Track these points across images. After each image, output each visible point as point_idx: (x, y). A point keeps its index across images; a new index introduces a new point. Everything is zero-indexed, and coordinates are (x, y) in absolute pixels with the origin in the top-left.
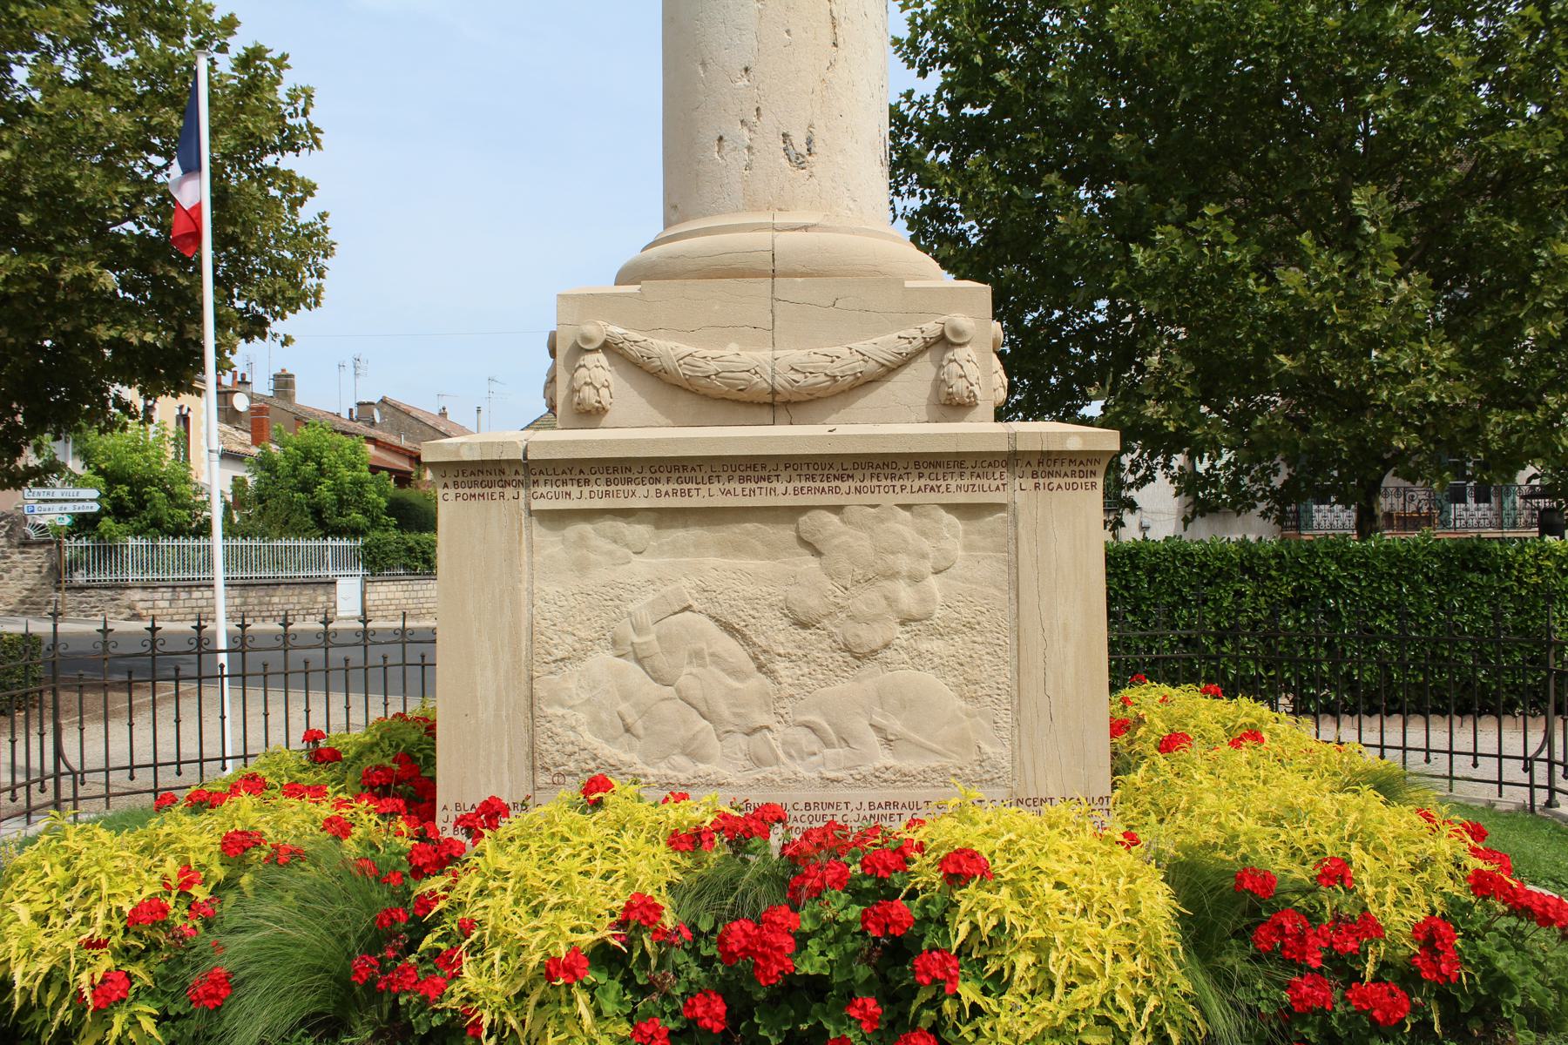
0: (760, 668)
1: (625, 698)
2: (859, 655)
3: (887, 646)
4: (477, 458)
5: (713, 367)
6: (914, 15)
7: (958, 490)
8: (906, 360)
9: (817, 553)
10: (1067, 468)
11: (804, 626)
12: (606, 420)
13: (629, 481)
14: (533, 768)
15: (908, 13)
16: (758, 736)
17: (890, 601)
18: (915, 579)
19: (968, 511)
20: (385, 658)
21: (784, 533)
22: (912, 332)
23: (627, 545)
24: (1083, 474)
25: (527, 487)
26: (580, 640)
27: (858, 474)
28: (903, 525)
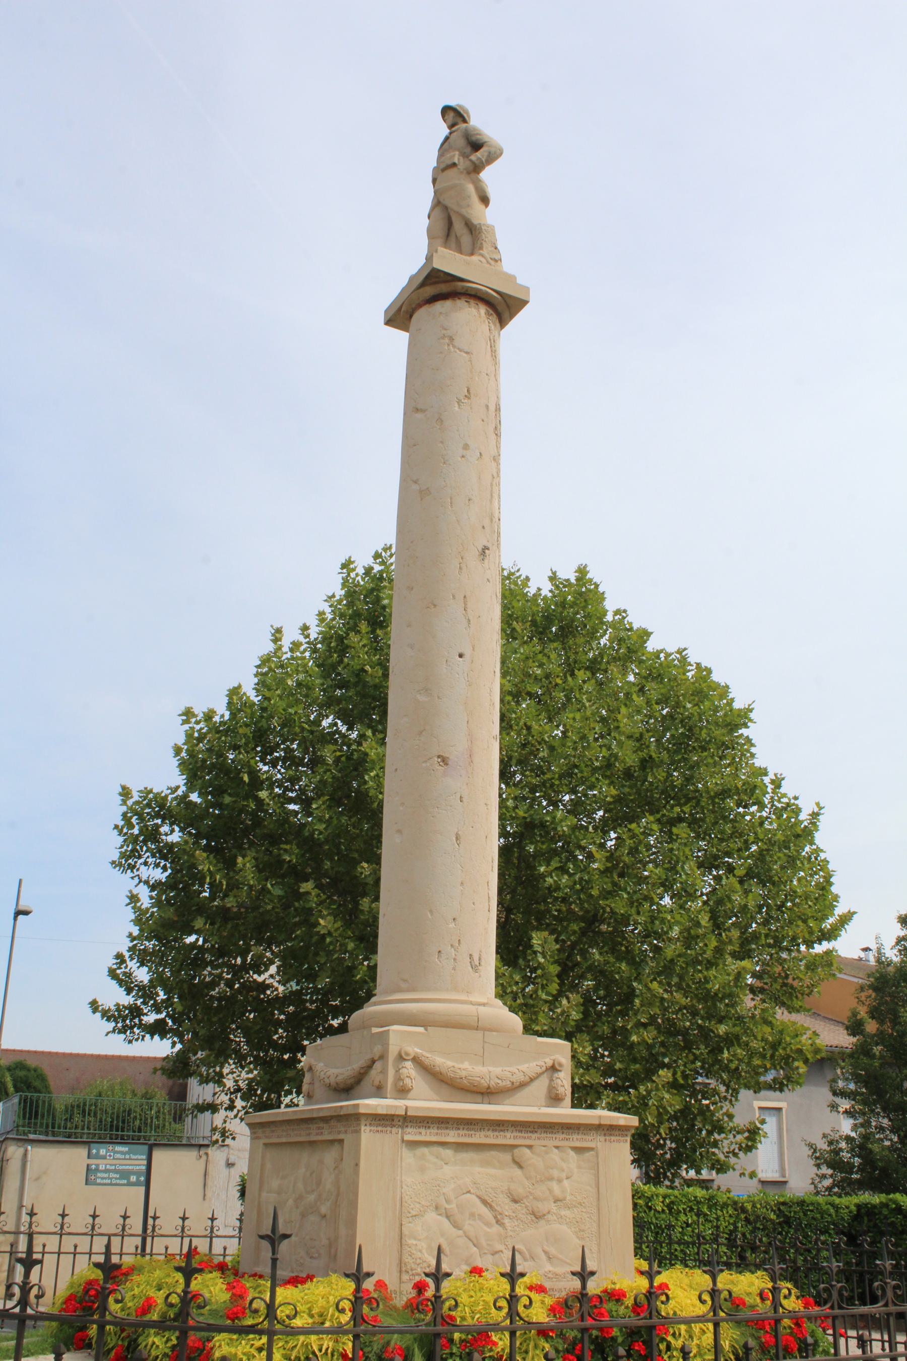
0: (497, 1222)
1: (442, 1235)
2: (537, 1216)
3: (549, 1213)
4: (385, 1112)
5: (463, 1074)
6: (192, 728)
7: (577, 1140)
8: (539, 1075)
9: (520, 1167)
10: (617, 1133)
11: (515, 1201)
12: (411, 1095)
13: (447, 1128)
14: (401, 1272)
15: (187, 727)
16: (497, 1256)
17: (551, 1191)
18: (560, 1181)
19: (579, 1150)
20: (76, 1247)
21: (506, 1157)
22: (541, 1063)
23: (442, 1160)
24: (623, 1136)
25: (402, 1128)
26: (423, 1206)
27: (539, 1131)
28: (555, 1155)
